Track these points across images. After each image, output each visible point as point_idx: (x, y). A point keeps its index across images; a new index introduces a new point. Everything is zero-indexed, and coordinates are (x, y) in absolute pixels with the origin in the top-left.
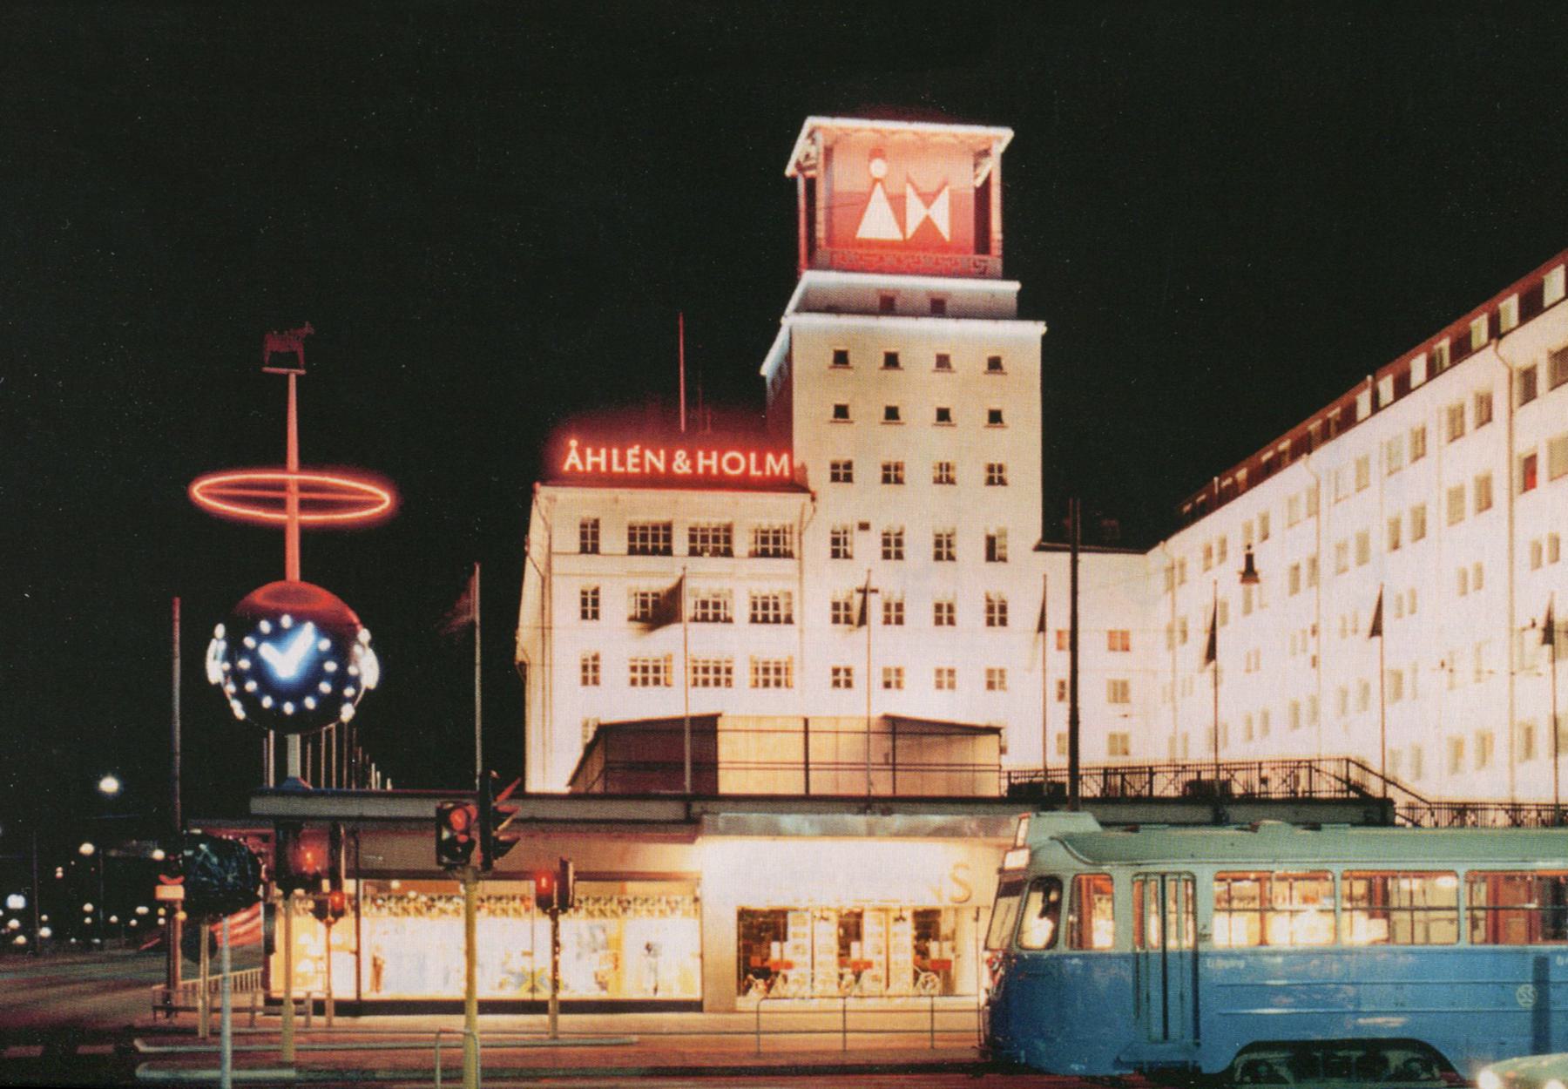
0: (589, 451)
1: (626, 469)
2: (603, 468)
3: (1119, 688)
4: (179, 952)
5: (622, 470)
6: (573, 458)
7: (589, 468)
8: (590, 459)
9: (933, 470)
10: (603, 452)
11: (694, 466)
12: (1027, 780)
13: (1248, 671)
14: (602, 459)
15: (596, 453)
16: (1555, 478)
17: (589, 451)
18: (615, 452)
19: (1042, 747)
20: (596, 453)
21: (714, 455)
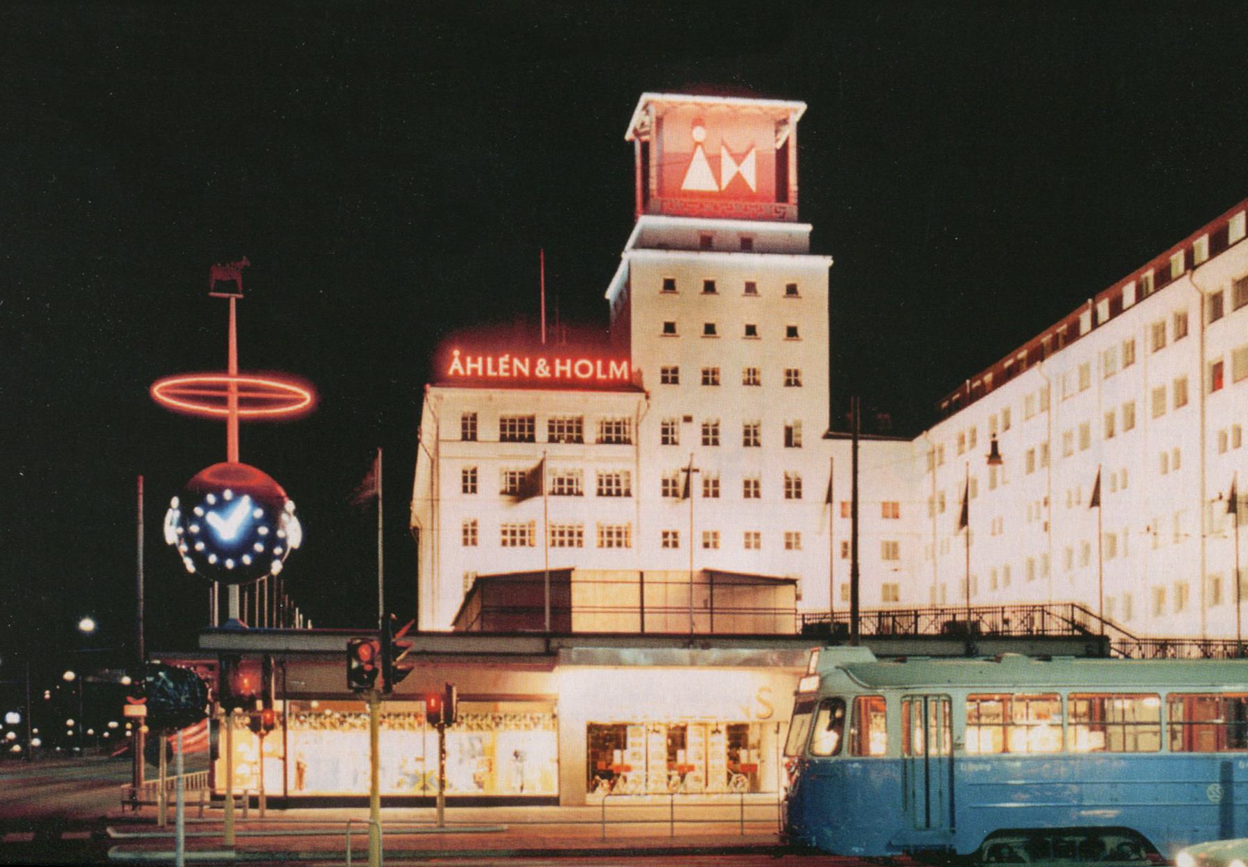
0: (469, 359)
1: (498, 373)
2: (480, 373)
3: (891, 547)
4: (143, 758)
5: (495, 374)
6: (456, 365)
7: (469, 373)
8: (470, 366)
9: (742, 374)
10: (480, 360)
11: (552, 371)
12: (817, 621)
13: (993, 534)
14: (479, 366)
15: (474, 361)
16: (1238, 381)
17: (469, 359)
18: (489, 360)
19: (829, 595)
20: (474, 361)
21: (569, 362)
